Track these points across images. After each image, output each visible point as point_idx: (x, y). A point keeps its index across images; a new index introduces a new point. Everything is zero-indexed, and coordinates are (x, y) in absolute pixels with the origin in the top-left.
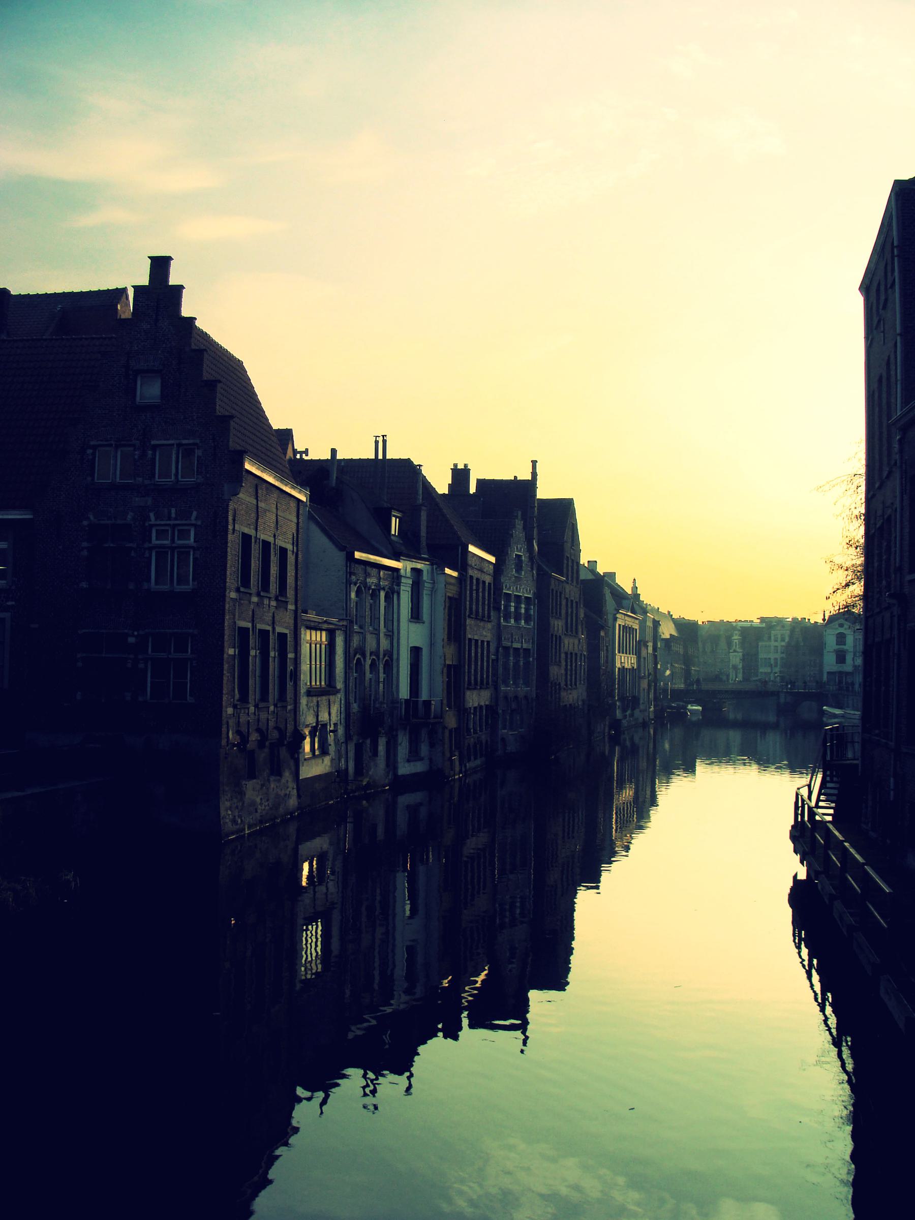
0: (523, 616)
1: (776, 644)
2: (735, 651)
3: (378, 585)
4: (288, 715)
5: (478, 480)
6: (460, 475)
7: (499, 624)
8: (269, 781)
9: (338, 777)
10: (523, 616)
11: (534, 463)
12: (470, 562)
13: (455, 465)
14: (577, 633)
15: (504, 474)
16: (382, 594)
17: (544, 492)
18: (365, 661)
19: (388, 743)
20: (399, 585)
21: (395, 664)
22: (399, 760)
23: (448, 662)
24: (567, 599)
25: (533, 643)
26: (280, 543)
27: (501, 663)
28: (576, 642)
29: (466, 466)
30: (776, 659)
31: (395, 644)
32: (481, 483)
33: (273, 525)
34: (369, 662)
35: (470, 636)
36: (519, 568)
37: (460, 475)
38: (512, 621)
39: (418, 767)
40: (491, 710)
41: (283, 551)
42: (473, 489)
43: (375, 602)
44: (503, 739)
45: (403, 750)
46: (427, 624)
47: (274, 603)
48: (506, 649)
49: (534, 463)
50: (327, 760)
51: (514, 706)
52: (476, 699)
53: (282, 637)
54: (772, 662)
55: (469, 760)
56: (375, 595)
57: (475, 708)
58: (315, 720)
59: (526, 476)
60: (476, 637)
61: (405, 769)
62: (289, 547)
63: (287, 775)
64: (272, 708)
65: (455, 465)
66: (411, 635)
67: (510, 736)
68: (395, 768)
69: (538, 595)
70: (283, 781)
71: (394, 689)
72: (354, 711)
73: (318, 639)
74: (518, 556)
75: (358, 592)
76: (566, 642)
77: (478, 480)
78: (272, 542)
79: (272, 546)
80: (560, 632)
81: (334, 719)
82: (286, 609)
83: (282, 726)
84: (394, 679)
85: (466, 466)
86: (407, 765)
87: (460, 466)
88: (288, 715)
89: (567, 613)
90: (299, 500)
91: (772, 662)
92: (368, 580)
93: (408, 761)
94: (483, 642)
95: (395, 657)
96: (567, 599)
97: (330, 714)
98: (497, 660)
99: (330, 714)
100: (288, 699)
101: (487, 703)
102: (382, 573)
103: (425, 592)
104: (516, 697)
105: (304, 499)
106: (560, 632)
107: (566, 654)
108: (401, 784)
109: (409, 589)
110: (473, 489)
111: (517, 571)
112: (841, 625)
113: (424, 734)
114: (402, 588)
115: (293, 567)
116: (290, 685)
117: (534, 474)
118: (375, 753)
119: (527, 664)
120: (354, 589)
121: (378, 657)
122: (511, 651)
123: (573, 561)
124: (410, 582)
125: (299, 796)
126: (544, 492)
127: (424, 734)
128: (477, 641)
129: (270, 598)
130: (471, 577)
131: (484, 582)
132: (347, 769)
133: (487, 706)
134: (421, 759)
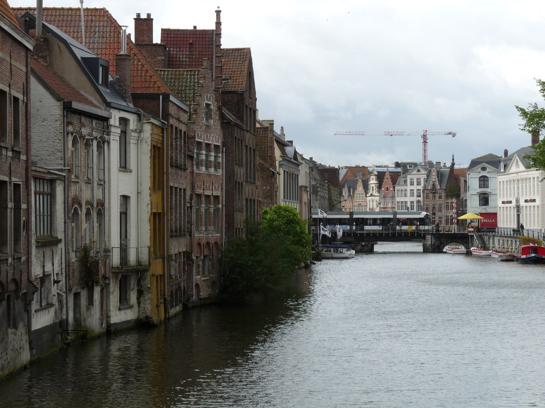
0: (213, 164)
1: (412, 187)
2: (372, 195)
3: (90, 134)
4: (22, 267)
5: (163, 31)
6: (144, 24)
7: (192, 172)
8: (7, 333)
9: (60, 326)
10: (213, 164)
11: (218, 12)
12: (170, 111)
13: (139, 15)
14: (254, 180)
15: (184, 24)
16: (95, 143)
17: (226, 43)
18: (81, 211)
19: (102, 291)
20: (109, 134)
21: (107, 214)
22: (111, 309)
23: (154, 211)
24: (246, 146)
25: (222, 189)
26: (14, 93)
27: (194, 210)
28: (254, 188)
29: (149, 15)
30: (412, 202)
31: (107, 194)
32: (166, 33)
33: (8, 74)
34: (84, 211)
35: (171, 184)
36: (209, 116)
37: (144, 24)
38: (204, 168)
39: (129, 315)
40: (187, 255)
41: (16, 100)
42: (157, 39)
43: (88, 152)
44: (197, 285)
45: (114, 298)
46: (134, 173)
47: (10, 154)
48: (199, 196)
49: (218, 12)
50: (52, 310)
51: (206, 252)
52: (177, 247)
53: (17, 186)
54: (409, 205)
55: (172, 307)
56: (88, 145)
57: (176, 254)
58: (42, 271)
59: (212, 26)
60: (176, 185)
61: (118, 317)
62: (20, 96)
63: (21, 325)
64: (10, 260)
65: (139, 15)
66: (120, 184)
67: (202, 283)
68: (108, 317)
69: (224, 144)
70: (18, 333)
71: (106, 239)
72: (73, 260)
73: (42, 190)
74: (208, 105)
75: (75, 142)
76: (247, 190)
77: (163, 31)
78: (8, 92)
79: (8, 95)
80: (242, 179)
81: (57, 269)
82: (19, 159)
83: (17, 278)
84: (106, 227)
85: (149, 15)
86: (118, 312)
87: (144, 16)
88: (22, 267)
89: (247, 160)
90: (27, 49)
91: (409, 205)
92: (83, 130)
93: (120, 309)
94: (180, 189)
95: (106, 206)
96: (246, 146)
97: (53, 265)
98: (191, 207)
99: (53, 265)
100: (22, 251)
101: (184, 250)
102: (94, 123)
103: (132, 141)
104: (208, 243)
105: (31, 48)
106: (242, 179)
107: (247, 199)
108: (111, 332)
109: (118, 138)
110: (157, 39)
111: (207, 119)
112: (484, 169)
113: (133, 282)
114: (112, 137)
115: (24, 117)
116: (23, 234)
117: (218, 24)
118: (91, 302)
119: (217, 210)
120: (70, 138)
121: (92, 206)
122: (212, 198)
123: (250, 109)
124: (119, 131)
125: (31, 349)
126: (226, 43)
127: (133, 282)
128: (176, 188)
129: (7, 148)
130: (172, 125)
131: (181, 131)
132: (67, 319)
133: (184, 252)
134: (131, 307)
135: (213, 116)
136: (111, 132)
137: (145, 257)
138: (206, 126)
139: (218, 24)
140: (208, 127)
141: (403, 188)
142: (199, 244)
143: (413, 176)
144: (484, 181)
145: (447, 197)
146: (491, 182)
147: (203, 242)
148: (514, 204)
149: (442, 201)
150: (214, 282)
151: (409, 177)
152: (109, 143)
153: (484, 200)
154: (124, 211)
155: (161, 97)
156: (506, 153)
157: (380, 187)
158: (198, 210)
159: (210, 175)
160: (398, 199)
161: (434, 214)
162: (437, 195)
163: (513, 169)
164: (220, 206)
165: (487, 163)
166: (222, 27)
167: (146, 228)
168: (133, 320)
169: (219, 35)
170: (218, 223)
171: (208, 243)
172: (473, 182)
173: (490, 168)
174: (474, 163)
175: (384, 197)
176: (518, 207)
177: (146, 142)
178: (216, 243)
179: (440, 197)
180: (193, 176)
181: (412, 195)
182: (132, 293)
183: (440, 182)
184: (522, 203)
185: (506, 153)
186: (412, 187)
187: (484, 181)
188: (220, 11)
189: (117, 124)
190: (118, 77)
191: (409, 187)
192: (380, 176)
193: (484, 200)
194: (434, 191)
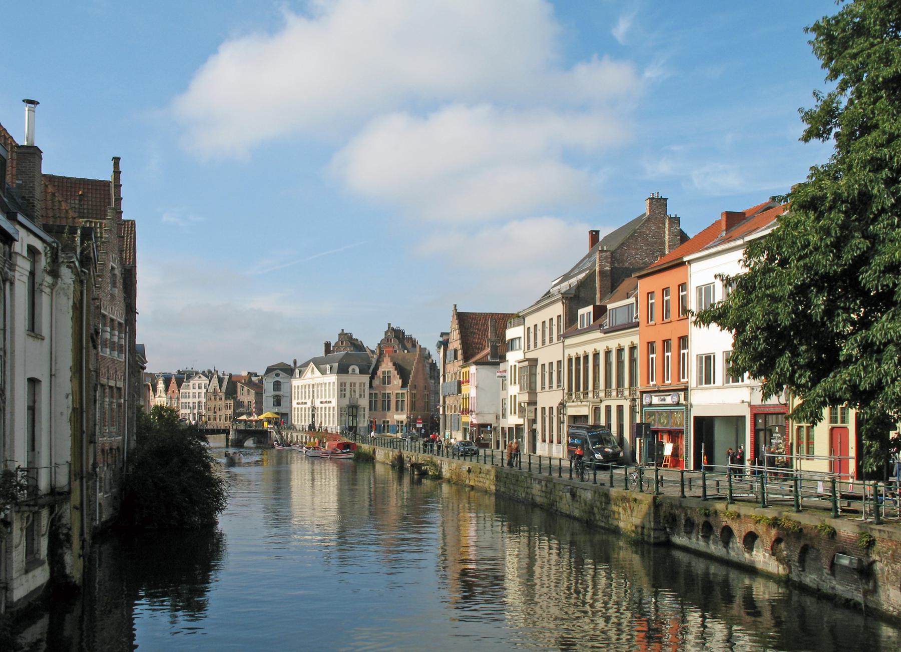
11: (116, 160)
22: (14, 576)
46: (47, 340)
49: (116, 160)
74: (113, 268)
112: (278, 375)
117: (117, 173)
122: (115, 390)
135: (118, 285)
136: (16, 265)
137: (62, 480)
138: (111, 295)
139: (117, 173)
140: (112, 296)
141: (187, 391)
142: (103, 451)
143: (195, 381)
144: (277, 386)
145: (226, 398)
146: (284, 387)
147: (107, 447)
148: (309, 405)
149: (222, 403)
150: (115, 498)
151: (191, 384)
152: (12, 284)
153: (278, 402)
154: (31, 404)
155: (79, 232)
156: (295, 362)
157: (166, 390)
158: (102, 407)
159: (113, 361)
160: (182, 400)
161: (215, 412)
162: (218, 397)
163: (308, 374)
164: (122, 401)
165: (281, 370)
166: (122, 176)
167: (65, 431)
168: (42, 585)
169: (118, 186)
170: (120, 422)
171: (111, 449)
172: (268, 386)
173: (282, 374)
174: (269, 370)
175: (171, 398)
176: (314, 409)
177: (66, 294)
178: (118, 448)
179: (221, 399)
180: (97, 359)
181: (194, 397)
182: (42, 539)
183: (220, 386)
184: (317, 404)
185: (295, 362)
186: (194, 391)
187: (277, 386)
188: (119, 159)
189: (25, 254)
190: (20, 182)
191: (191, 391)
192: (167, 382)
193: (278, 402)
194: (215, 393)
